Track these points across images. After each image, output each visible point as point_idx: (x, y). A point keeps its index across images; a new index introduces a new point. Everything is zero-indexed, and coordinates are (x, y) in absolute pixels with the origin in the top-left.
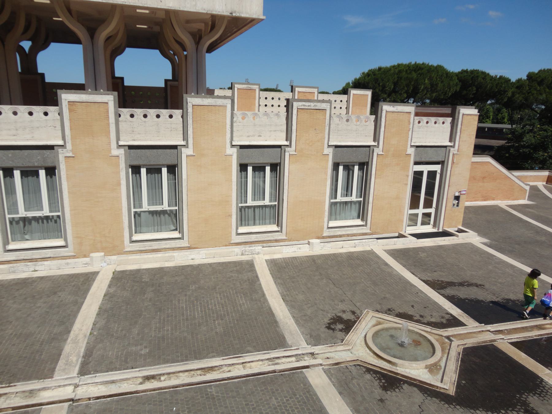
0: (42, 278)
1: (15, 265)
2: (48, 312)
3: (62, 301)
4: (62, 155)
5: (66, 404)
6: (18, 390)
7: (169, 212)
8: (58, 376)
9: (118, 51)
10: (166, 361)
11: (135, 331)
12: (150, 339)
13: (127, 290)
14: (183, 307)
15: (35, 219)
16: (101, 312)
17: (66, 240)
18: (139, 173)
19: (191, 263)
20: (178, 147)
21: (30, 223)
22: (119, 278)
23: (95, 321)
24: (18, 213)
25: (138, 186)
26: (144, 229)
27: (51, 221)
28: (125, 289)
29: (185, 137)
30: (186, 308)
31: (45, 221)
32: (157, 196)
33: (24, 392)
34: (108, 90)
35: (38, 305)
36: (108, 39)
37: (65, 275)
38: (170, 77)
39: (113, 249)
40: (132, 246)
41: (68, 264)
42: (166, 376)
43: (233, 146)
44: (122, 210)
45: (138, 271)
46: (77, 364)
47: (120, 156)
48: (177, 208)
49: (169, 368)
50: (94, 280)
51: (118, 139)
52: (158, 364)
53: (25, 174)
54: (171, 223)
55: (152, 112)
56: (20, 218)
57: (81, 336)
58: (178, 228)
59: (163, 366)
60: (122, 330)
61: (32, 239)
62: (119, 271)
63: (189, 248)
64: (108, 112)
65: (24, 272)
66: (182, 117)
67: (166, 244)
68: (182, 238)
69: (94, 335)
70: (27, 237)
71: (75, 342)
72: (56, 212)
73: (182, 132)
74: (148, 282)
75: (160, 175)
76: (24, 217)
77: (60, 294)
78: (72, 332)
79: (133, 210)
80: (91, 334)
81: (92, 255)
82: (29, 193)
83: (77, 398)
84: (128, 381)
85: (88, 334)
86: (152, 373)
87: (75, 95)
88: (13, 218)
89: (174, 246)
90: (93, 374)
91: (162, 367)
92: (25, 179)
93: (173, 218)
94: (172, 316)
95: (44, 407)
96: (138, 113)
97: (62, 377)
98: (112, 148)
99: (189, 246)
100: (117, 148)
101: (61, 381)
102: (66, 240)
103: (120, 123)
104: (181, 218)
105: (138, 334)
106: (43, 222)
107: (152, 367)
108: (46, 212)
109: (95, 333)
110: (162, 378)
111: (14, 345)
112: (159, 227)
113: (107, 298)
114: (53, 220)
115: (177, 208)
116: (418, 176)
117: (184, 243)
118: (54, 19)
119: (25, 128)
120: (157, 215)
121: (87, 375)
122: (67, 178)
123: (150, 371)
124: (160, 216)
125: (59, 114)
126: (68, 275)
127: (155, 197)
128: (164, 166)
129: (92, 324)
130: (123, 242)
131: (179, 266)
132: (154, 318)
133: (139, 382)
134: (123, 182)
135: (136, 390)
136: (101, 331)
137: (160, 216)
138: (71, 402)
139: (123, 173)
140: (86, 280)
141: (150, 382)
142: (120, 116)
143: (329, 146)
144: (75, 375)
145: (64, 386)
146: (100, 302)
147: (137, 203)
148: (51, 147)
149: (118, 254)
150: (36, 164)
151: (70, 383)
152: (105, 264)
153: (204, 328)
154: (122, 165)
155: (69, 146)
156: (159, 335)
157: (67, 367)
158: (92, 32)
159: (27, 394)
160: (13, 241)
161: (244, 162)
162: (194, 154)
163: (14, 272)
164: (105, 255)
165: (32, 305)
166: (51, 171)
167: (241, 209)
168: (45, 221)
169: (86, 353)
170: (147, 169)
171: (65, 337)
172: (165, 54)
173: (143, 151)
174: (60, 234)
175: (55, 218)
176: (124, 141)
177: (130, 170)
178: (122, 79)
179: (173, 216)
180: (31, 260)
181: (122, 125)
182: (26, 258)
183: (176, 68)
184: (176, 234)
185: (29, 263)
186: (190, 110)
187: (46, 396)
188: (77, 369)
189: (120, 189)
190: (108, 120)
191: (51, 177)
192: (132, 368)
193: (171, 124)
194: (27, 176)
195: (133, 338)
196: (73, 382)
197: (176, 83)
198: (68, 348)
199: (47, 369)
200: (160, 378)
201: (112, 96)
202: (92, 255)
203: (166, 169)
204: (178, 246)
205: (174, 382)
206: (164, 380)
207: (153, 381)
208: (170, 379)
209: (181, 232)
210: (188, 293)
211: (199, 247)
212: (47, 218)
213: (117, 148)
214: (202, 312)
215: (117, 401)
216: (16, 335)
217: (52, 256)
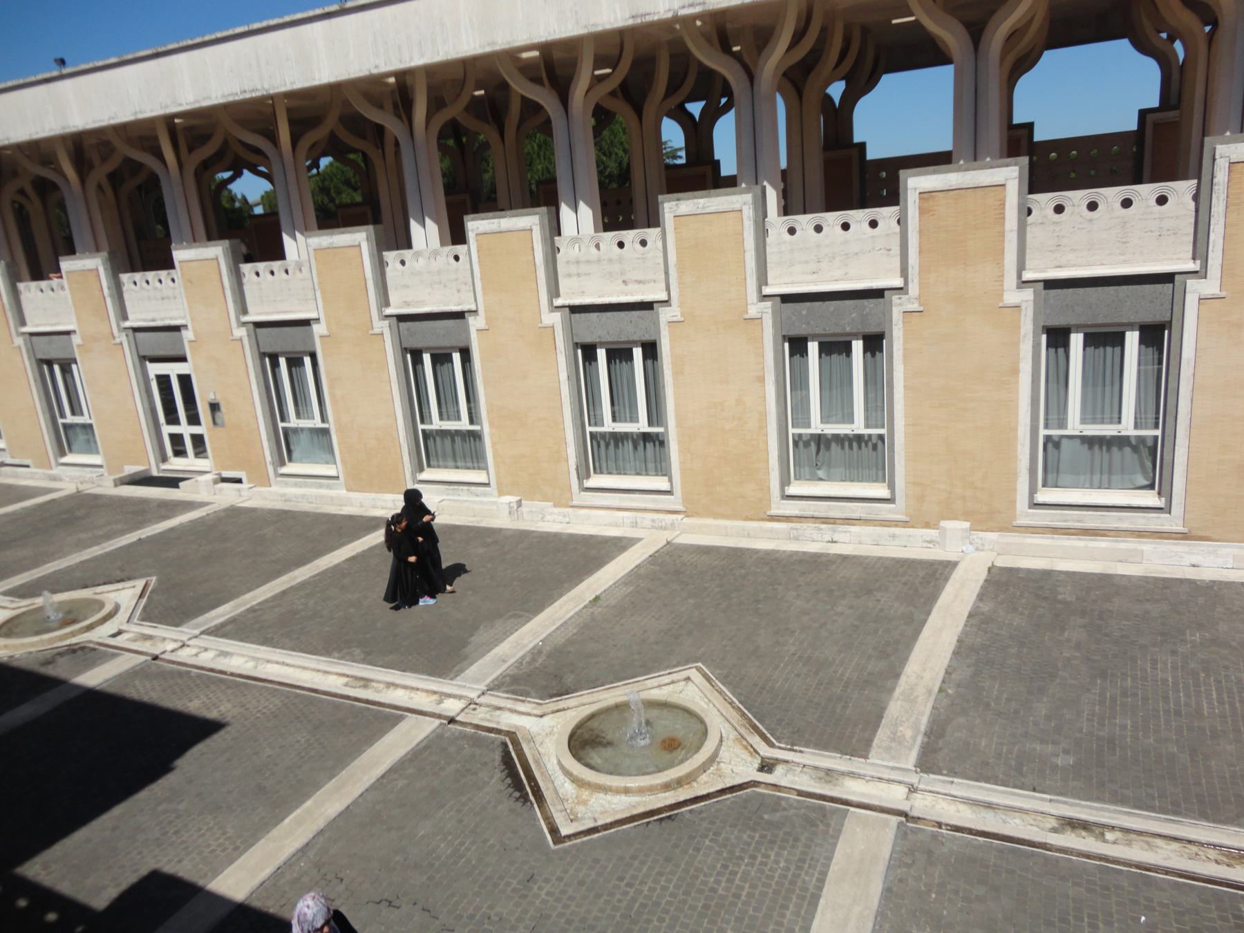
0: (845, 558)
1: (798, 525)
2: (856, 627)
3: (882, 610)
4: (898, 306)
5: (894, 820)
6: (807, 762)
7: (1134, 442)
8: (877, 760)
9: (1023, 63)
10: (1119, 799)
11: (1041, 708)
12: (1078, 735)
13: (1022, 614)
14: (1165, 681)
15: (838, 439)
16: (962, 650)
17: (892, 487)
18: (1066, 345)
19: (1190, 574)
20: (886, 293)
21: (828, 448)
22: (1002, 582)
23: (949, 666)
24: (809, 426)
25: (1059, 378)
26: (1064, 478)
27: (866, 445)
28: (1016, 609)
29: (1200, 249)
30: (1175, 684)
31: (855, 444)
32: (1107, 400)
33: (816, 768)
34: (1001, 157)
35: (839, 609)
36: (1013, 36)
37: (887, 558)
38: (1154, 102)
39: (992, 518)
40: (1034, 515)
41: (894, 536)
42: (1118, 834)
43: (1023, 284)
44: (1016, 430)
45: (1047, 574)
46: (913, 745)
47: (1023, 307)
48: (1158, 433)
49: (1126, 818)
50: (947, 579)
51: (763, 280)
52: (1098, 799)
53: (827, 348)
54: (1138, 468)
55: (1110, 195)
56: (812, 435)
57: (920, 691)
58: (1158, 479)
59: (1112, 807)
60: (1009, 700)
61: (829, 478)
62: (1001, 569)
63: (1185, 536)
64: (1003, 205)
65: (814, 541)
66: (1196, 198)
67: (1120, 519)
68: (1167, 509)
69: (947, 695)
70: (821, 473)
71: (910, 698)
72: (876, 427)
73: (1191, 238)
74: (1071, 603)
75: (1118, 349)
76: (819, 435)
77: (879, 595)
78: (903, 678)
79: (1043, 432)
80: (941, 690)
81: (944, 524)
82: (830, 389)
83: (915, 813)
84: (1024, 816)
85: (936, 689)
86: (1083, 816)
87: (935, 177)
88: (800, 435)
89: (1141, 527)
90: (947, 775)
91: (1109, 811)
92: (1090, 350)
93: (1149, 460)
94: (1135, 695)
95: (852, 809)
96: (1076, 201)
97: (885, 763)
98: (1005, 287)
99: (1185, 530)
100: (1019, 287)
101: (883, 770)
102: (892, 487)
103: (1028, 229)
104: (1167, 458)
105: (1048, 718)
106: (851, 447)
107: (1083, 803)
108: (858, 426)
109: (950, 691)
110: (1109, 836)
111: (798, 675)
112: (1105, 477)
113: (974, 621)
114: (870, 445)
115: (1158, 433)
116: (164, 381)
117: (1171, 522)
118: (894, 22)
119: (834, 258)
120: (1101, 448)
121: (934, 773)
122: (905, 356)
123: (1077, 809)
124: (1108, 450)
125: (899, 222)
126: (893, 559)
127: (837, 405)
128: (1131, 326)
129: (943, 671)
130: (1012, 503)
131: (1156, 579)
132: (1088, 690)
133: (1049, 826)
134: (1026, 367)
135: (1043, 841)
136: (962, 690)
137: (1108, 450)
138: (903, 819)
139: (1027, 344)
140: (933, 576)
141: (1078, 836)
142: (1030, 212)
143: (766, 297)
144: (910, 766)
145: (889, 781)
146: (960, 628)
147: (1053, 417)
148: (878, 293)
149: (1001, 530)
150: (848, 329)
151: (901, 779)
152: (971, 548)
153: (1229, 748)
154: (1027, 326)
155: (914, 289)
156: (1101, 734)
157: (893, 745)
158: (976, 32)
159: (822, 774)
160: (796, 479)
161: (1058, 321)
162: (1223, 294)
163: (796, 539)
164: (972, 529)
165: (828, 607)
166: (874, 343)
167: (1052, 443)
168: (855, 444)
169: (932, 729)
170: (821, 344)
171: (889, 684)
172: (1143, 47)
173: (1081, 291)
174: (880, 473)
175: (874, 441)
176: (1035, 270)
177: (1044, 337)
178: (1030, 127)
179: (1145, 453)
180: (826, 520)
181: (1033, 234)
182: (816, 514)
183: (1175, 76)
184: (1150, 498)
185: (823, 526)
186: (1221, 176)
187: (853, 789)
188: (914, 755)
189: (1017, 382)
190: (1003, 224)
191: (873, 355)
192: (1034, 790)
193: (1161, 219)
194: (829, 353)
195: (1035, 724)
196: (906, 779)
197: (1171, 115)
198: (894, 708)
199: (856, 737)
200: (1103, 834)
201: (1017, 168)
202: (943, 523)
203: (1136, 334)
204: (1153, 527)
205: (1137, 853)
206: (1114, 843)
207: (1084, 833)
208: (1129, 843)
209: (1166, 491)
210: (1181, 649)
211: (1214, 536)
212: (859, 438)
213: (1019, 287)
214: (1221, 703)
215: (1001, 851)
216: (801, 658)
217: (864, 516)
